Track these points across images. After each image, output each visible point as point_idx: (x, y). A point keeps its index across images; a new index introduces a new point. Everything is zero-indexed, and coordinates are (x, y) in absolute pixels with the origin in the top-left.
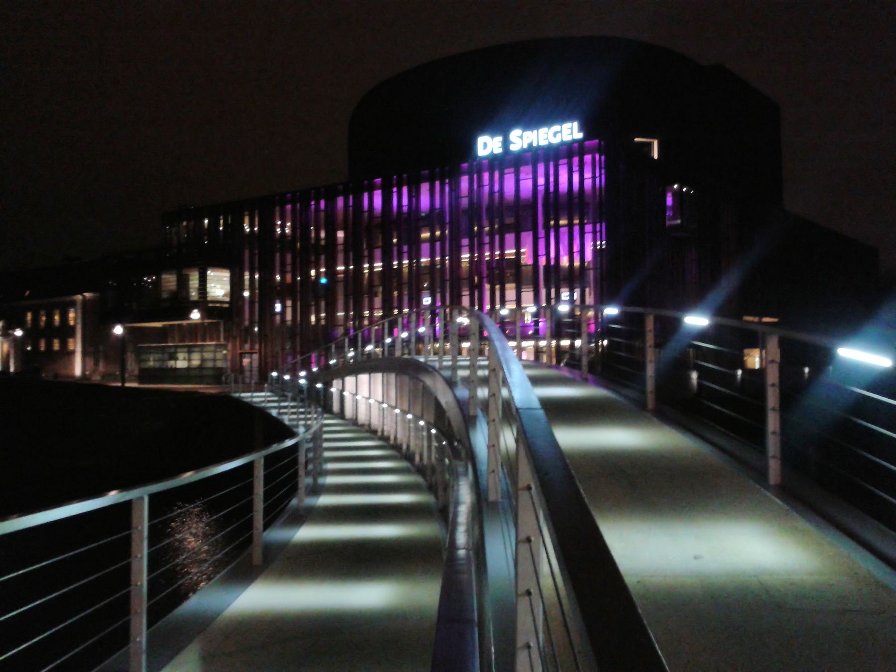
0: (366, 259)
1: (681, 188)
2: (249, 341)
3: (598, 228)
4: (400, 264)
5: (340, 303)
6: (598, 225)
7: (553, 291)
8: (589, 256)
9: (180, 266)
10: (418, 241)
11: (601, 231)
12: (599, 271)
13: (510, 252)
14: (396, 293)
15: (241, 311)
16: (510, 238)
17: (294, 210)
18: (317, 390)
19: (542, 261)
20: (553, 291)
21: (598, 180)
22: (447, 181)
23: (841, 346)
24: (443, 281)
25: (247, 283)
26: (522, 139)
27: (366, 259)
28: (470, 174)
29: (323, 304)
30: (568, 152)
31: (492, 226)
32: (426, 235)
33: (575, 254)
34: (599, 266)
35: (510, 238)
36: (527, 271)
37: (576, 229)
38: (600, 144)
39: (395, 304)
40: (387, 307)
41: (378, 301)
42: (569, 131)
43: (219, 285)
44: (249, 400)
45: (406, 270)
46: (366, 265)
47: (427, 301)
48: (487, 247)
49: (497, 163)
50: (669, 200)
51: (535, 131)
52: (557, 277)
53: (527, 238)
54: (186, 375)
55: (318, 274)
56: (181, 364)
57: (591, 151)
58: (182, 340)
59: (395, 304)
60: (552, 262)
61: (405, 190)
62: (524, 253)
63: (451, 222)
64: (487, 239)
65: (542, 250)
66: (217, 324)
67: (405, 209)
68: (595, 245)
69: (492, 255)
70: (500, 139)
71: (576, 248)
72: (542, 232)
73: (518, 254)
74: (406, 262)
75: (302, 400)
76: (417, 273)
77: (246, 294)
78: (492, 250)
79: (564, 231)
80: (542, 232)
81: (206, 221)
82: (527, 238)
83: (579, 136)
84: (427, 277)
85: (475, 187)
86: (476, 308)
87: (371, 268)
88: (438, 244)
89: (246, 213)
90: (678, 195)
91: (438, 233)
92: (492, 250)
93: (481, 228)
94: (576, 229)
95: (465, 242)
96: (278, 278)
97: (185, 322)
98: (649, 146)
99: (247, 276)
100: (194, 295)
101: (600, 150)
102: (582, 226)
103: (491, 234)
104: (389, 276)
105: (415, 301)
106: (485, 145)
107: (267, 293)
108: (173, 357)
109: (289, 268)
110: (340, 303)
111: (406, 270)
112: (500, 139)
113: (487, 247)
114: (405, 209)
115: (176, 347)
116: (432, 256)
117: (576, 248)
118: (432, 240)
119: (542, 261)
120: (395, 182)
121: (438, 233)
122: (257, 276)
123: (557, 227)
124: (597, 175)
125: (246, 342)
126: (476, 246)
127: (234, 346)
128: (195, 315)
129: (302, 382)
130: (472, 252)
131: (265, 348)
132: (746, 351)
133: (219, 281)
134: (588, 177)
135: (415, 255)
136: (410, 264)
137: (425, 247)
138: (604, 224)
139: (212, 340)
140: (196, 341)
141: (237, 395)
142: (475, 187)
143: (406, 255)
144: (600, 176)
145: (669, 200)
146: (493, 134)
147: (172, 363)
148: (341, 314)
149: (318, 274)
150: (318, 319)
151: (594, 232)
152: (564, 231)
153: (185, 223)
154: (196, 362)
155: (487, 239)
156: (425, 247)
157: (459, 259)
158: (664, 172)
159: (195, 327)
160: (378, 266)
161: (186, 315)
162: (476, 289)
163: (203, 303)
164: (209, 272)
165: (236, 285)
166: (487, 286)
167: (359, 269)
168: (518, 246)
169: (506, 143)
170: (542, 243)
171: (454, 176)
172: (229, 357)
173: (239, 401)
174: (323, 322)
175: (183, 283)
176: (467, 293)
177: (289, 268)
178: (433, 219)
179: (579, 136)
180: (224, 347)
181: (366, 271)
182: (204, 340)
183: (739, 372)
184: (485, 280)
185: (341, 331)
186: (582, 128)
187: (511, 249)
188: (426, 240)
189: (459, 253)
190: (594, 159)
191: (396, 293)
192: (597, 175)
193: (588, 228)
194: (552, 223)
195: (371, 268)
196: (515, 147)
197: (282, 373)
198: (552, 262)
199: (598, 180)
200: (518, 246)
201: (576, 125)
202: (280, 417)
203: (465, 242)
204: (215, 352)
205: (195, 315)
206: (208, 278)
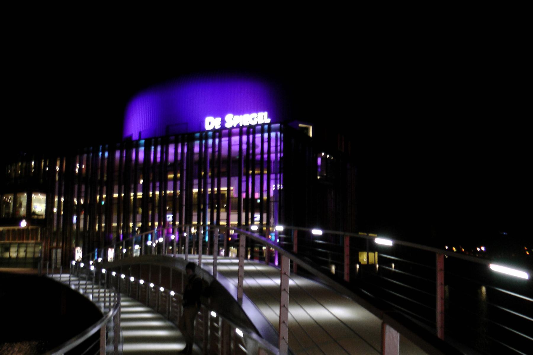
0: (132, 190)
1: (326, 155)
2: (56, 240)
3: (279, 177)
4: (154, 194)
5: (115, 217)
6: (279, 175)
7: (250, 214)
8: (272, 194)
9: (16, 191)
10: (166, 180)
11: (280, 179)
12: (278, 203)
13: (224, 189)
14: (150, 212)
15: (52, 220)
16: (224, 180)
17: (88, 158)
18: (103, 275)
19: (244, 195)
20: (250, 214)
21: (279, 148)
22: (186, 143)
23: (491, 263)
24: (181, 205)
25: (56, 204)
26: (232, 120)
27: (132, 190)
28: (200, 139)
29: (103, 218)
30: (262, 129)
31: (213, 172)
32: (171, 176)
33: (245, 190)
34: (278, 200)
35: (224, 180)
36: (234, 201)
37: (265, 177)
38: (280, 126)
39: (150, 219)
40: (145, 221)
41: (139, 217)
42: (262, 118)
43: (39, 204)
44: (58, 279)
45: (157, 198)
46: (132, 194)
47: (170, 218)
48: (209, 185)
49: (219, 133)
50: (319, 161)
51: (241, 116)
52: (251, 206)
53: (235, 181)
54: (17, 262)
55: (101, 198)
56: (14, 255)
57: (275, 130)
58: (14, 239)
59: (150, 219)
60: (250, 196)
61: (258, 157)
62: (232, 190)
63: (187, 169)
64: (209, 181)
65: (244, 188)
66: (37, 230)
67: (158, 160)
68: (276, 187)
69: (212, 191)
70: (219, 120)
71: (265, 188)
72: (244, 178)
73: (229, 190)
74: (157, 193)
75: (102, 284)
76: (164, 199)
77: (55, 210)
78: (212, 188)
79: (258, 178)
80: (244, 178)
81: (33, 163)
82: (235, 181)
83: (268, 121)
84: (171, 203)
85: (203, 150)
86: (202, 223)
87: (135, 195)
88: (178, 183)
89: (59, 158)
90: (324, 159)
91: (179, 175)
92: (212, 188)
93: (206, 174)
94: (265, 177)
95: (196, 182)
96: (75, 201)
97: (16, 228)
98: (307, 129)
99: (56, 199)
100: (23, 211)
101: (280, 130)
102: (269, 175)
103: (212, 177)
104: (146, 201)
105: (162, 218)
106: (210, 123)
107: (69, 209)
108: (8, 250)
109: (83, 194)
110: (115, 217)
111: (157, 198)
112: (219, 120)
113: (209, 185)
114: (158, 160)
115: (10, 244)
116: (175, 189)
117: (265, 188)
118: (175, 179)
119: (244, 195)
120: (153, 143)
121: (179, 175)
122: (62, 200)
123: (253, 175)
124: (279, 144)
125: (54, 241)
126: (202, 185)
127: (46, 243)
128: (24, 224)
129: (92, 268)
130: (199, 188)
131: (66, 245)
132: (360, 253)
133: (39, 201)
134: (272, 144)
135: (163, 188)
136: (160, 194)
137: (170, 184)
138: (282, 175)
139: (32, 239)
140: (23, 240)
141: (50, 276)
142: (203, 150)
143: (158, 188)
144: (280, 146)
145: (319, 161)
146: (215, 116)
147: (7, 255)
148: (115, 224)
149: (101, 198)
150: (100, 227)
151: (276, 179)
152: (258, 178)
153: (20, 164)
154: (22, 254)
155: (209, 181)
156: (170, 184)
157: (191, 192)
158: (317, 144)
159: (24, 230)
160: (140, 195)
161: (18, 223)
162: (202, 212)
163: (30, 215)
164: (33, 195)
165: (49, 204)
166: (208, 211)
167: (127, 196)
168: (229, 186)
169: (223, 122)
170: (244, 185)
171: (191, 140)
172: (43, 251)
173: (52, 281)
174: (103, 230)
175: (17, 203)
176: (196, 214)
177: (83, 194)
178: (175, 167)
179: (268, 121)
180: (40, 244)
181: (132, 198)
182: (28, 239)
183: (358, 266)
184: (207, 206)
185: (114, 236)
186: (269, 116)
187: (224, 186)
188: (171, 180)
189: (192, 188)
190: (276, 135)
191: (150, 212)
192: (279, 144)
193: (273, 176)
194: (251, 172)
195: (135, 195)
196: (228, 125)
197: (137, 278)
198: (250, 196)
199: (279, 148)
200: (229, 186)
201: (266, 114)
202: (86, 295)
203: (196, 182)
204: (35, 247)
205: (24, 224)
206: (45, 202)
